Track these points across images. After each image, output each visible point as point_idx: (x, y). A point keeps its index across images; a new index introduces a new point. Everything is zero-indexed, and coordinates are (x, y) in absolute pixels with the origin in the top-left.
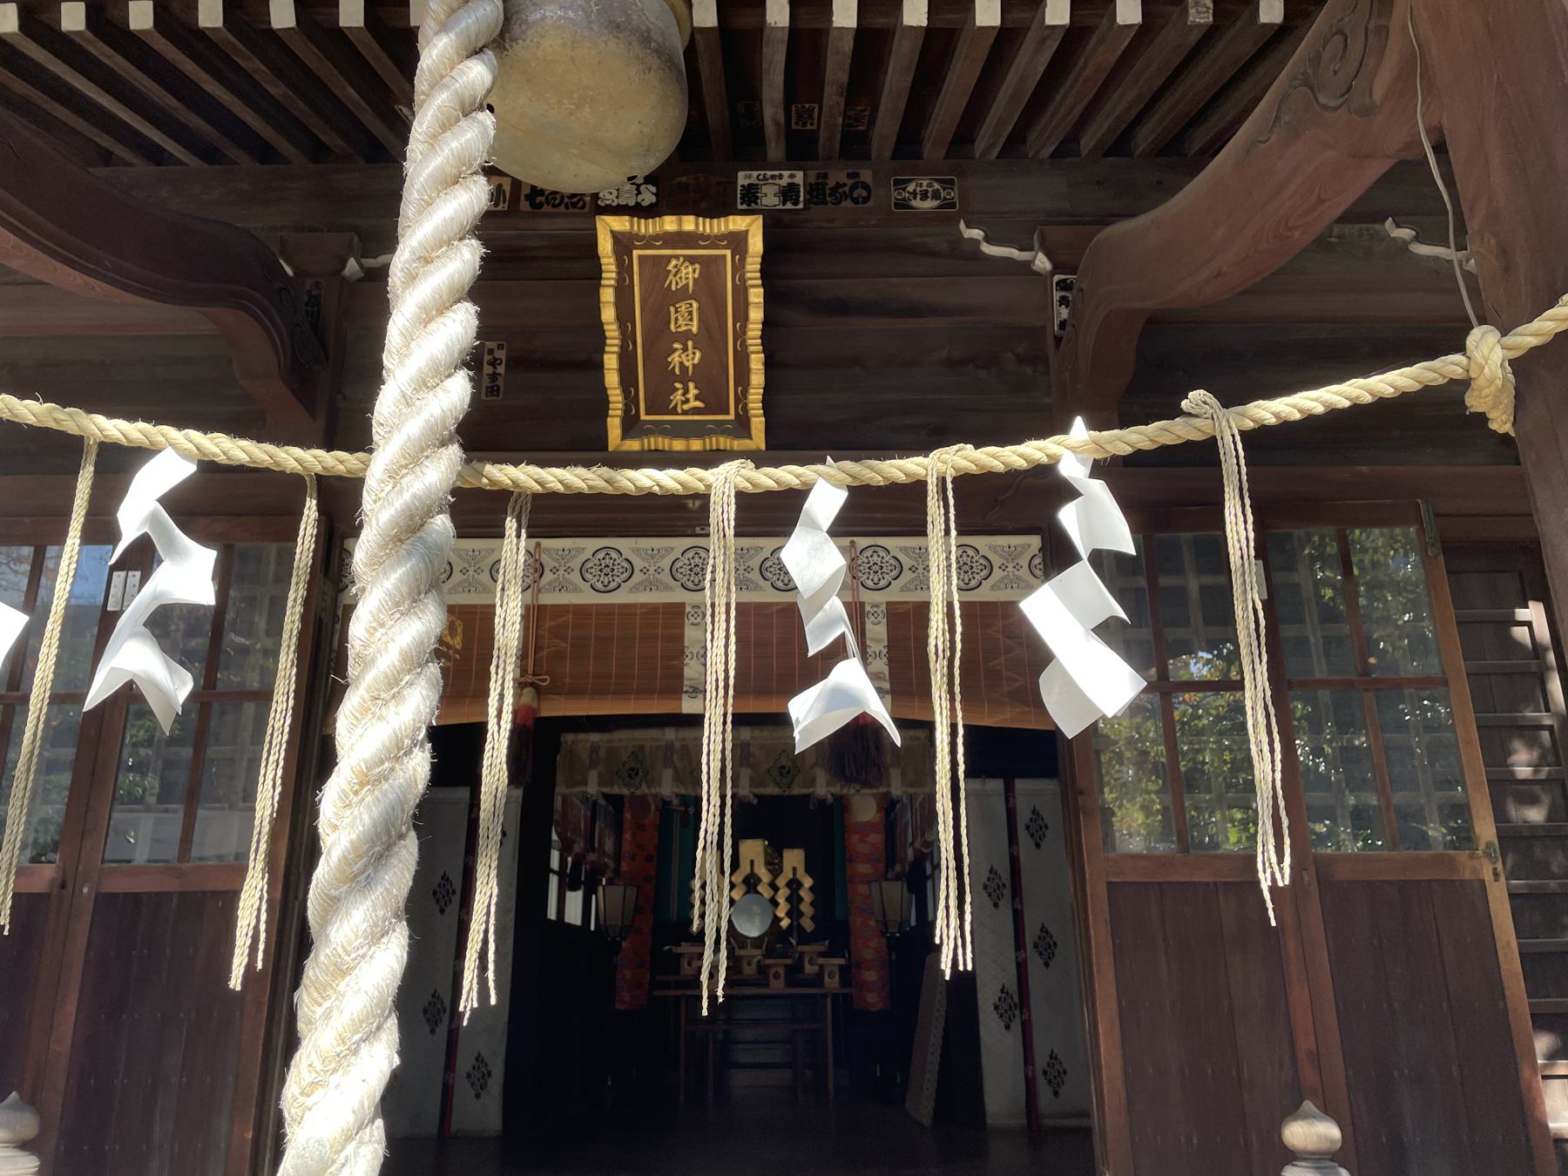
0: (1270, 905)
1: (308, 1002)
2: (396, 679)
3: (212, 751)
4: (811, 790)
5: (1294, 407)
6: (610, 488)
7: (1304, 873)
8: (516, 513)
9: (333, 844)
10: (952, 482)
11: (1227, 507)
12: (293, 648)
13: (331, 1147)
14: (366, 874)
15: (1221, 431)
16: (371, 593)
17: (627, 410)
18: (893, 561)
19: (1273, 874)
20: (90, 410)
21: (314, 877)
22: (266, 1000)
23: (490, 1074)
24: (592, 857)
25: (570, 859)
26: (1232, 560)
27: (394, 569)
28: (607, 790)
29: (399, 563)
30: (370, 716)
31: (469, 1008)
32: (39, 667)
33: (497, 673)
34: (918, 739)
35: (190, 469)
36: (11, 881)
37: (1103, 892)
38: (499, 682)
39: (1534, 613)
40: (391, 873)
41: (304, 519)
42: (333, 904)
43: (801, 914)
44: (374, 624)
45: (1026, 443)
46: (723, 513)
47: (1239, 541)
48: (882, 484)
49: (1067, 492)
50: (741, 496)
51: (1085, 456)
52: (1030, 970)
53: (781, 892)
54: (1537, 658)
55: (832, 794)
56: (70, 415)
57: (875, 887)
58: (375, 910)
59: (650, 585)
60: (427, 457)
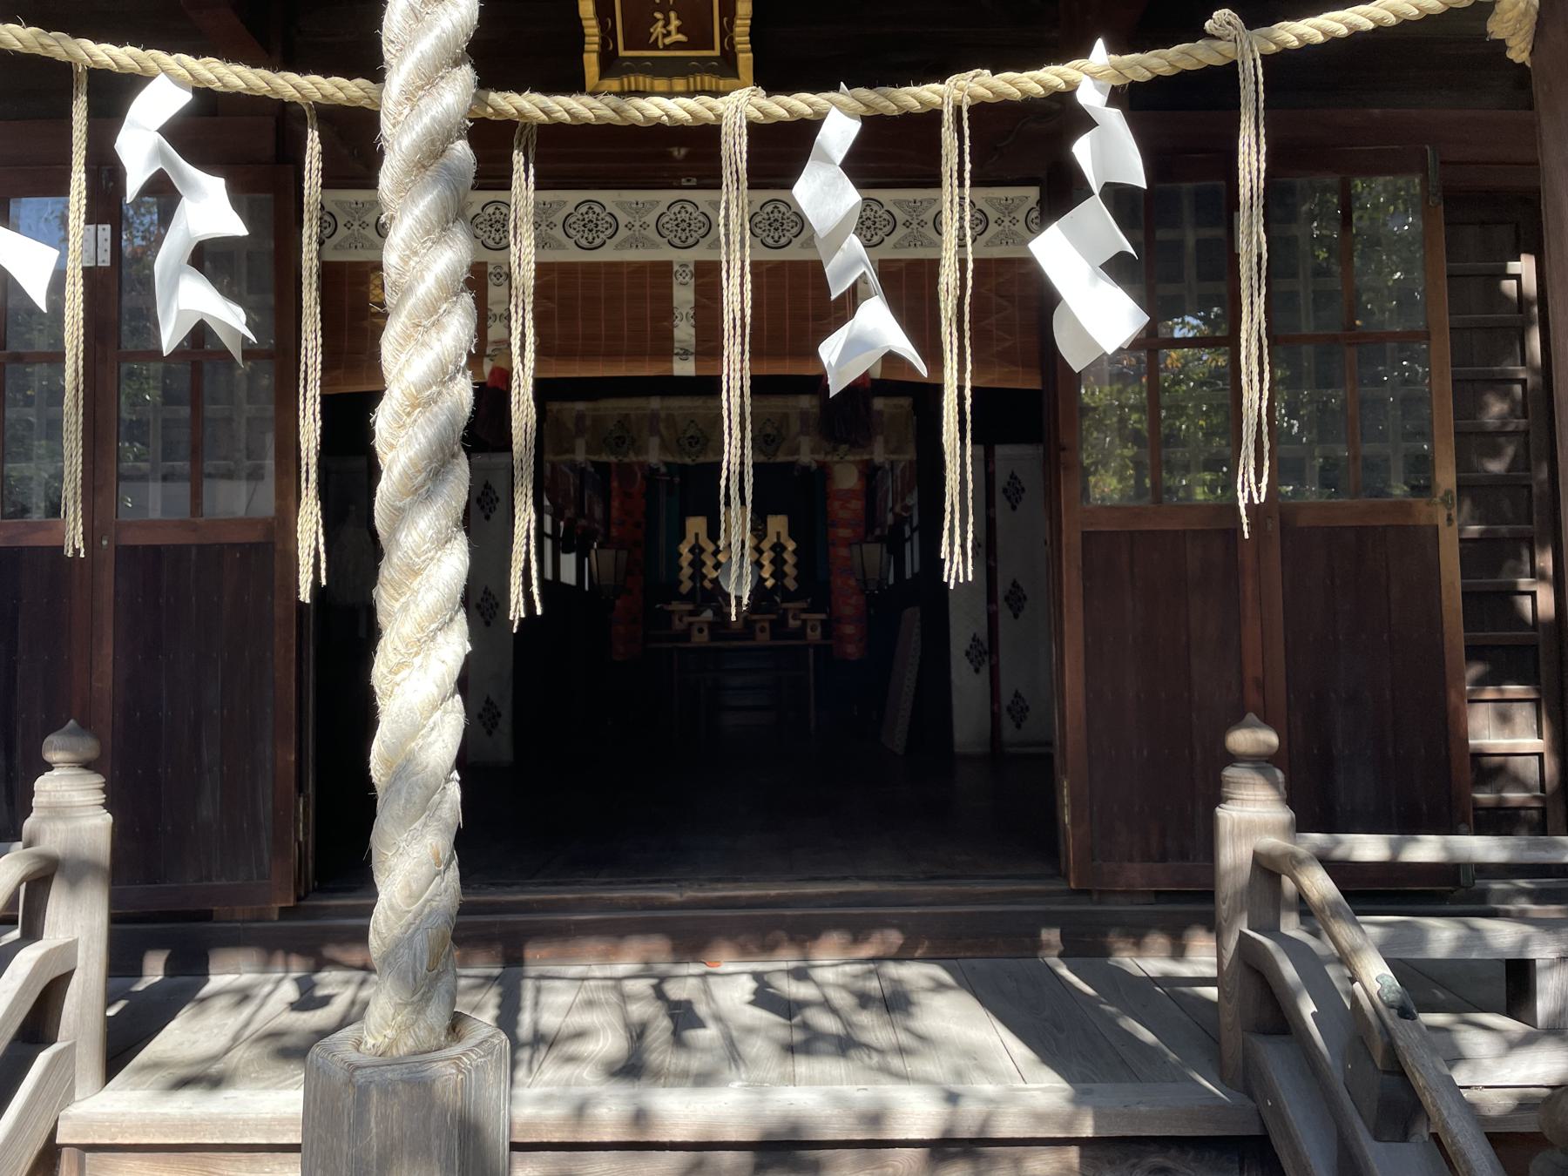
0: (1245, 520)
1: (387, 600)
2: (434, 307)
3: (210, 410)
4: (796, 457)
5: (1318, 28)
6: (618, 118)
7: (1269, 521)
8: (522, 146)
9: (393, 461)
10: (968, 111)
11: (1241, 137)
12: (314, 286)
13: (421, 714)
14: (426, 487)
15: (1243, 55)
16: (401, 221)
17: (604, 44)
18: (886, 216)
19: (1250, 493)
20: (76, 33)
21: (378, 491)
22: (293, 641)
23: (499, 715)
24: (583, 522)
25: (562, 524)
26: (1241, 191)
27: (422, 198)
28: (595, 458)
29: (425, 190)
30: (413, 343)
31: (517, 617)
32: (67, 305)
33: (516, 312)
34: (902, 406)
35: (185, 98)
36: (79, 509)
37: (1077, 539)
38: (520, 321)
39: (1525, 266)
40: (448, 488)
41: (308, 152)
42: (399, 515)
43: (785, 575)
44: (407, 252)
45: (1045, 69)
46: (735, 149)
47: (1250, 173)
48: (896, 113)
49: (1084, 122)
50: (754, 129)
51: (1103, 83)
52: (1001, 622)
53: (765, 555)
54: (1520, 311)
55: (817, 461)
56: (56, 39)
57: (856, 549)
58: (438, 520)
59: (635, 242)
60: (442, 78)
